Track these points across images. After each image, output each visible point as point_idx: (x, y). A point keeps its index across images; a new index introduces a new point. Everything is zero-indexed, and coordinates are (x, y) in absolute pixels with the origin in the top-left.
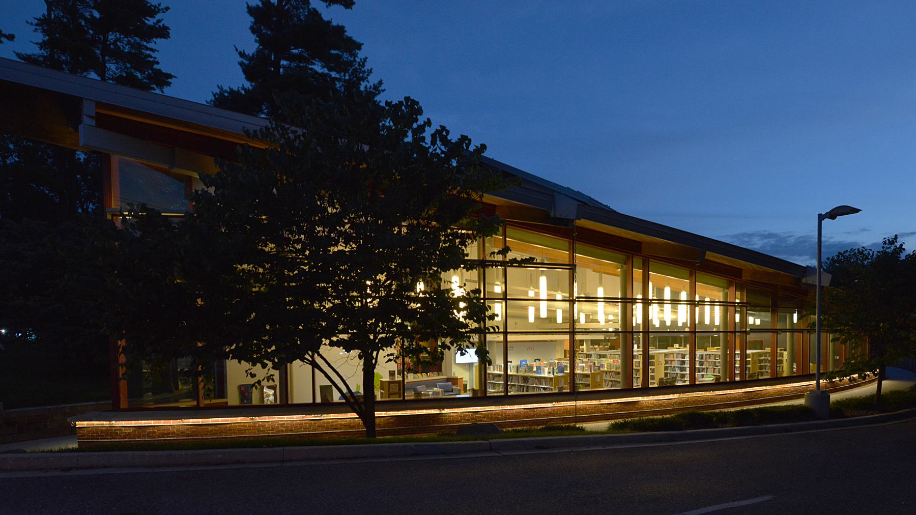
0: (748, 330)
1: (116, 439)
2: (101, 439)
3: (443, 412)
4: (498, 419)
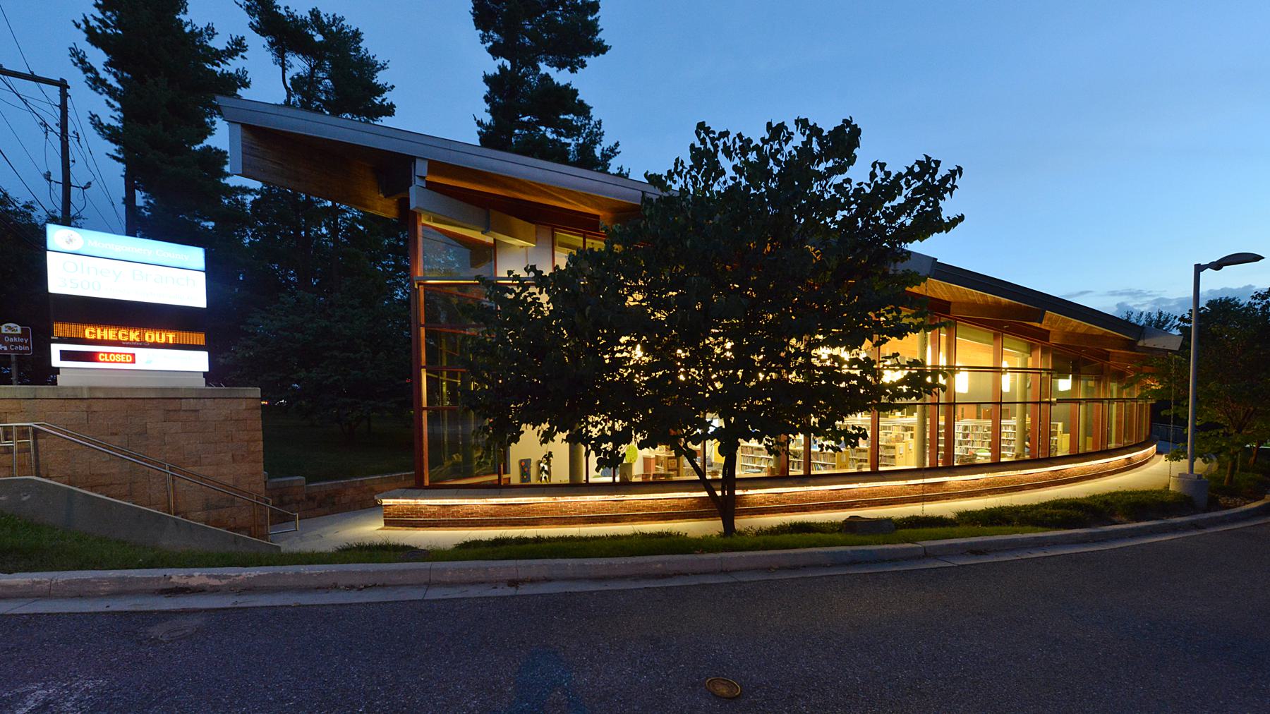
0: (1054, 399)
1: (421, 518)
2: (407, 517)
3: (746, 493)
4: (803, 501)
